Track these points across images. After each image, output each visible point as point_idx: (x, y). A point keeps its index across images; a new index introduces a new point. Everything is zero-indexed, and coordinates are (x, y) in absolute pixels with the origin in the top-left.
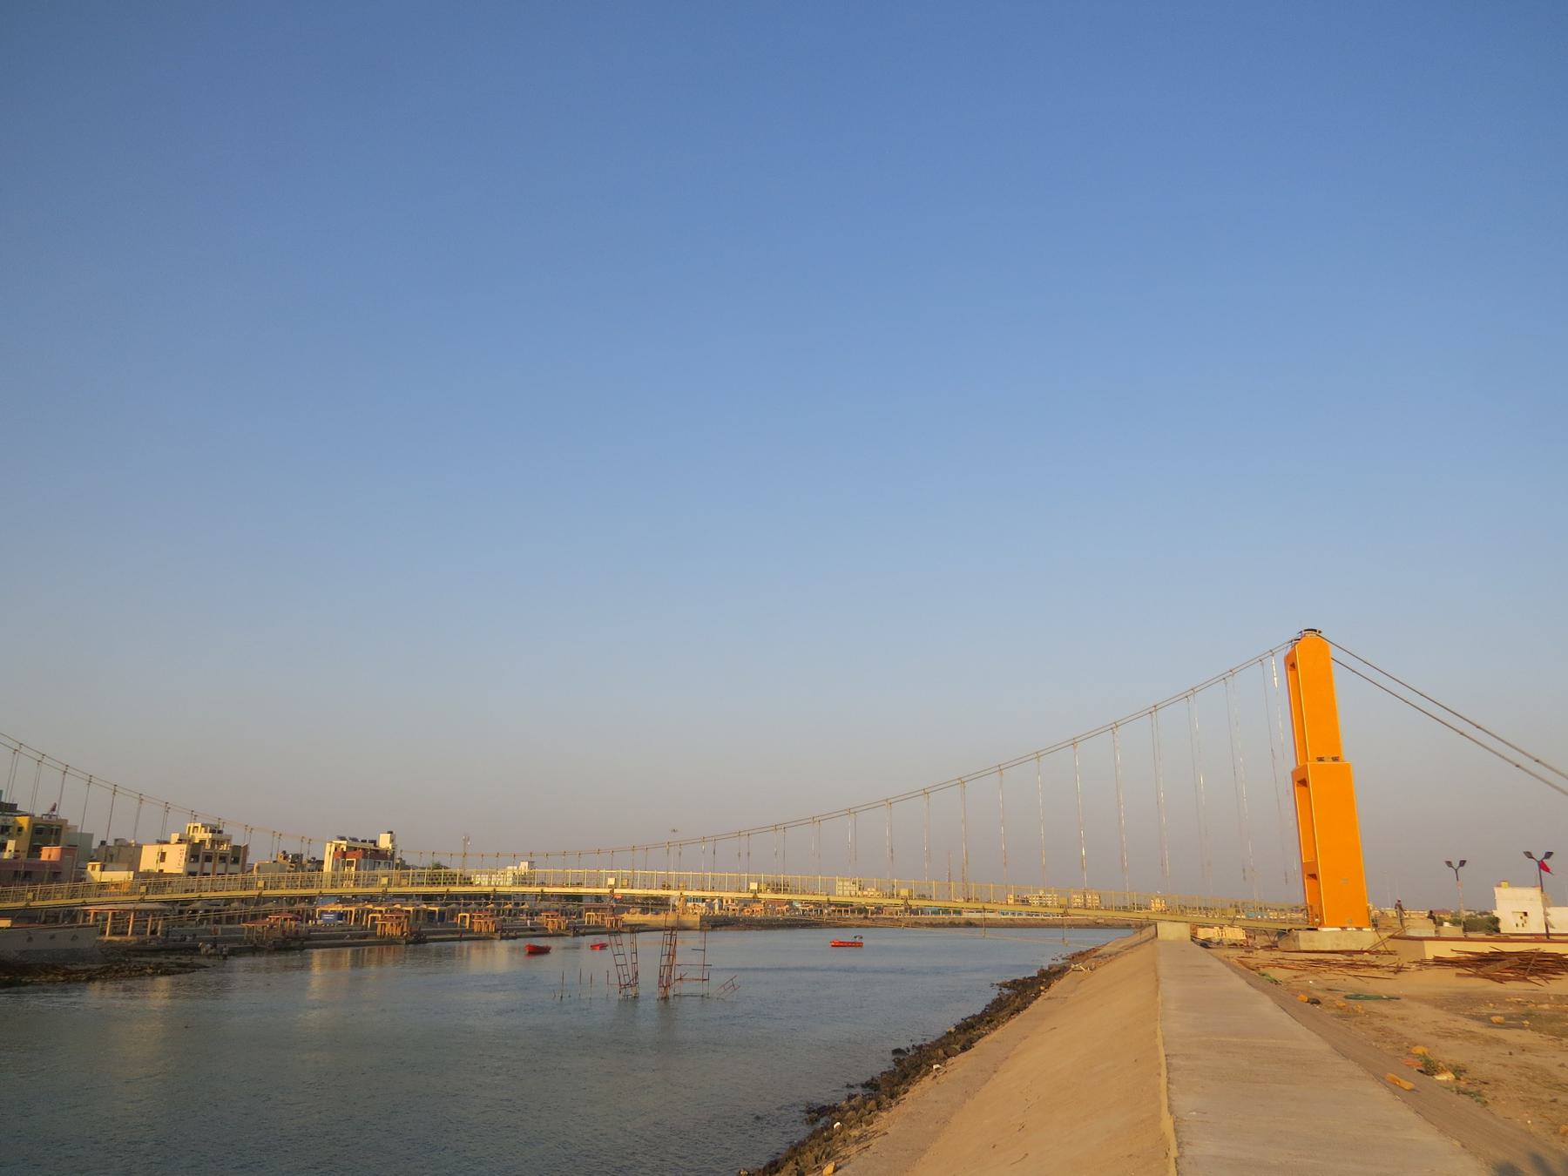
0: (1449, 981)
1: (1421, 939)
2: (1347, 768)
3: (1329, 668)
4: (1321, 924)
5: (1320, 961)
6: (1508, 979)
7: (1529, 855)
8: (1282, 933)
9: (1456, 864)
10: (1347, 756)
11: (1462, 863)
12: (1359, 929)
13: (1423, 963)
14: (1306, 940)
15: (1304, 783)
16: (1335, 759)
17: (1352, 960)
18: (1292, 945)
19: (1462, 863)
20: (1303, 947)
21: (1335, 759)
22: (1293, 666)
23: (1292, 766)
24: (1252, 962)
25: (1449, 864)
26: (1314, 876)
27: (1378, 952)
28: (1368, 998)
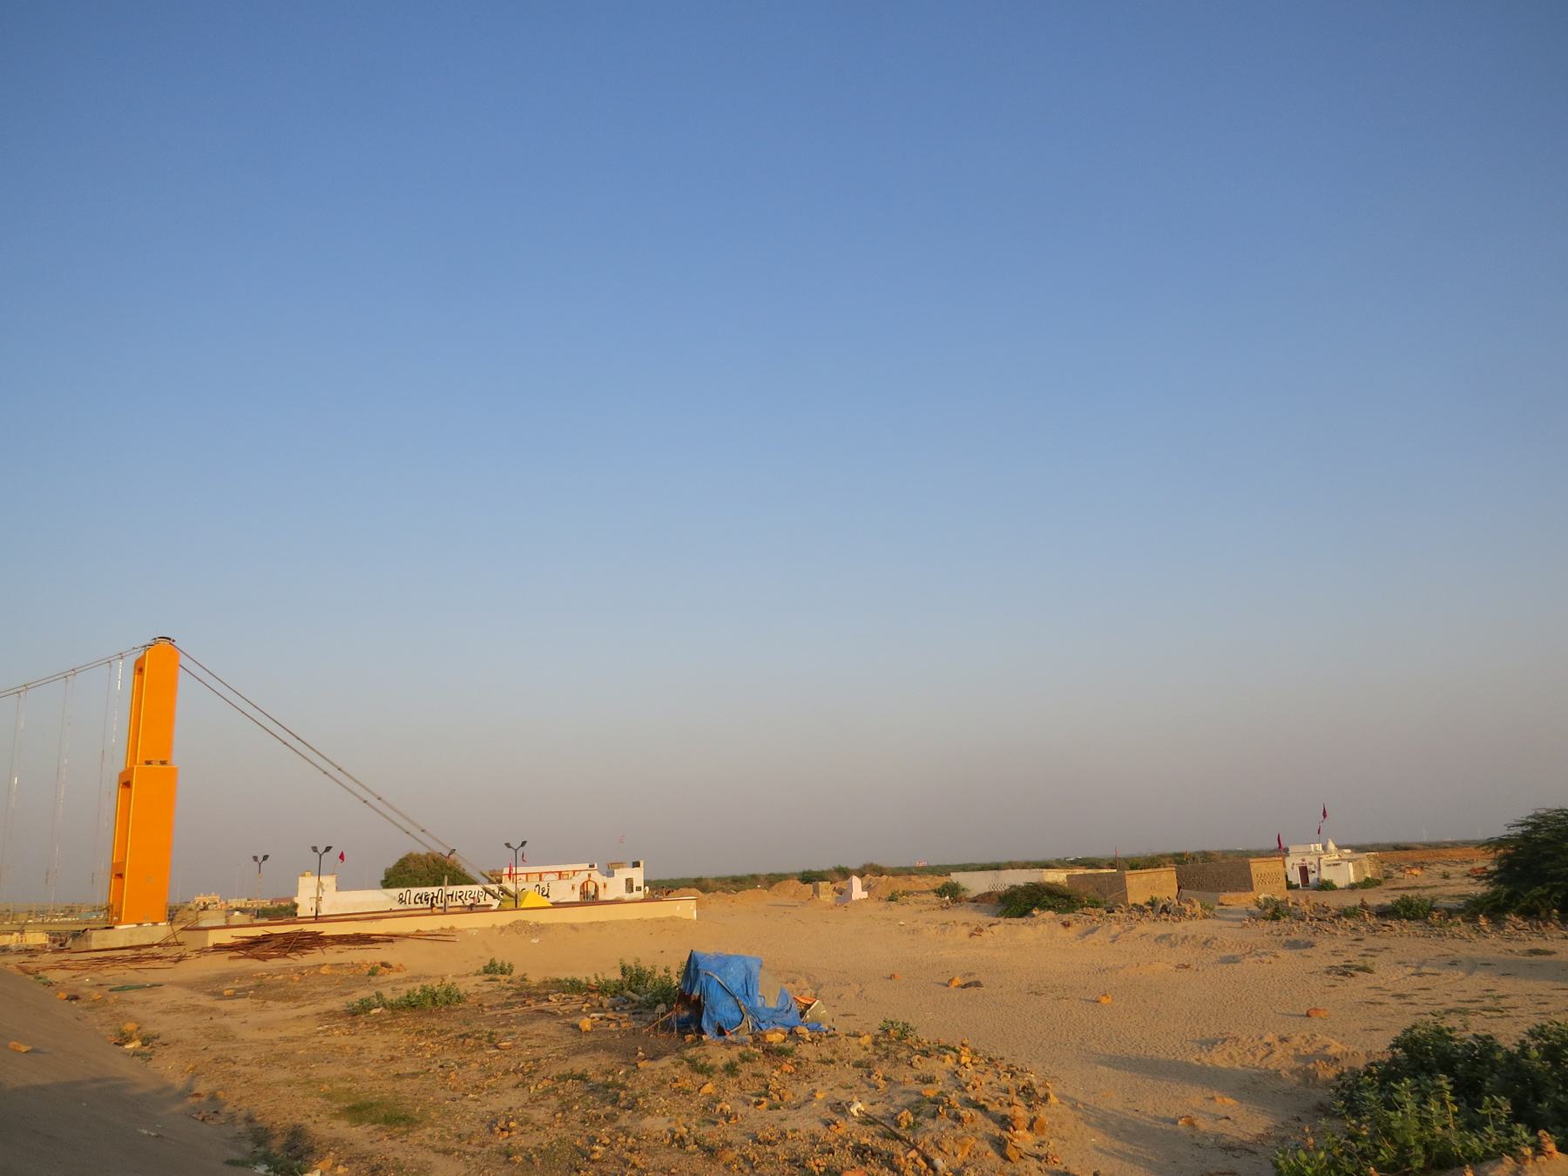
0: (222, 963)
1: (206, 929)
2: (174, 771)
3: (175, 678)
4: (119, 922)
5: (109, 958)
6: (271, 957)
7: (508, 845)
8: (76, 935)
9: (321, 849)
10: (177, 760)
11: (265, 858)
12: (155, 924)
13: (203, 951)
14: (98, 940)
15: (127, 785)
16: (163, 763)
17: (139, 955)
18: (84, 945)
19: (265, 858)
20: (94, 946)
21: (163, 763)
22: (141, 670)
23: (121, 768)
24: (32, 966)
25: (315, 849)
26: (120, 876)
27: (167, 944)
28: (131, 988)
